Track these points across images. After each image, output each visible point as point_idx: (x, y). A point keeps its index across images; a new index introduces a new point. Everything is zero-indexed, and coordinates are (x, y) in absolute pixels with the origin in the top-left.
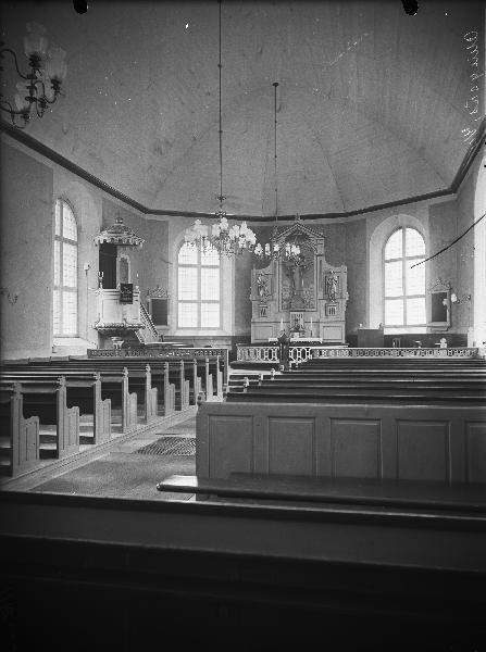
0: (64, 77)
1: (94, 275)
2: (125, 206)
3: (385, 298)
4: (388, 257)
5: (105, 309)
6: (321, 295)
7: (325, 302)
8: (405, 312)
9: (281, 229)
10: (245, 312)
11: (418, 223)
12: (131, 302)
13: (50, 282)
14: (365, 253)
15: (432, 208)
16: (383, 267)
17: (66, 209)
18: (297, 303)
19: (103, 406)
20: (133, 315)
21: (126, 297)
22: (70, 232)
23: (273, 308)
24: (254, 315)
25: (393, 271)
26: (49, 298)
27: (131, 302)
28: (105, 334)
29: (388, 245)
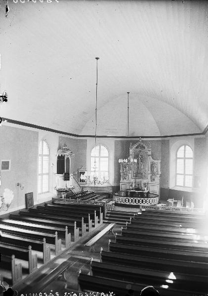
0: (31, 274)
1: (55, 169)
2: (69, 136)
3: (177, 174)
4: (178, 157)
5: (59, 182)
6: (149, 172)
7: (151, 175)
8: (184, 181)
9: (134, 143)
10: (118, 177)
11: (189, 144)
12: (69, 180)
13: (36, 171)
14: (169, 153)
15: (196, 139)
16: (176, 176)
17: (45, 144)
18: (139, 175)
19: (58, 241)
20: (71, 184)
21: (67, 178)
22: (46, 152)
23: (130, 175)
24: (122, 179)
25: (180, 162)
26: (36, 180)
27: (69, 180)
28: (60, 191)
29: (179, 151)
